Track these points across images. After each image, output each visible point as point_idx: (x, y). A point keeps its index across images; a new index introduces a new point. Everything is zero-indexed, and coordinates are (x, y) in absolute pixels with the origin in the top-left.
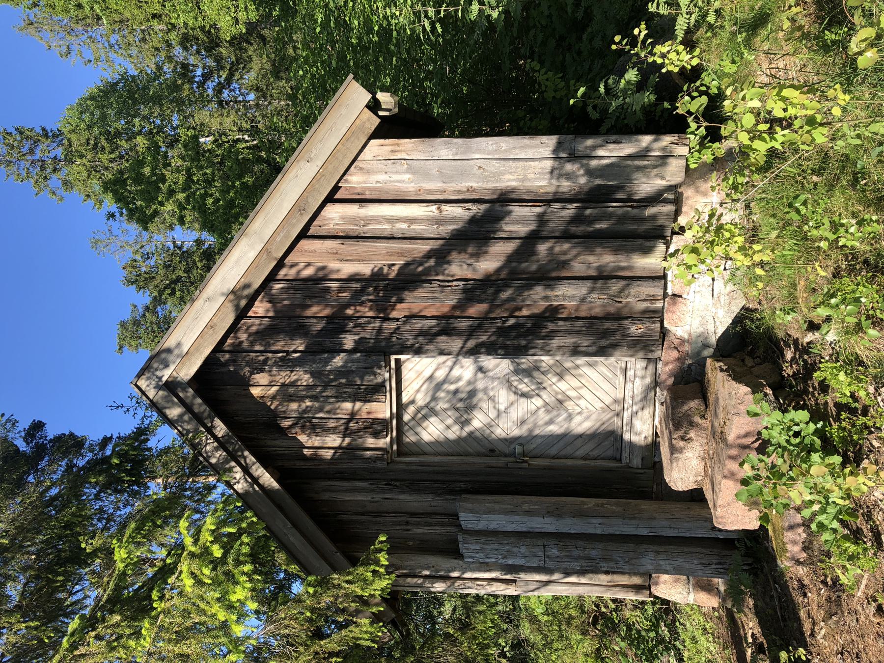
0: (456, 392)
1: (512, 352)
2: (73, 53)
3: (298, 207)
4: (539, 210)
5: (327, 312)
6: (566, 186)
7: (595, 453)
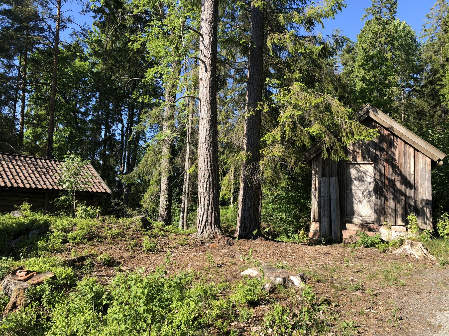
0: (363, 177)
1: (375, 190)
2: (428, 20)
3: (414, 142)
4: (413, 197)
5: (385, 148)
6: (419, 203)
7: (348, 210)
